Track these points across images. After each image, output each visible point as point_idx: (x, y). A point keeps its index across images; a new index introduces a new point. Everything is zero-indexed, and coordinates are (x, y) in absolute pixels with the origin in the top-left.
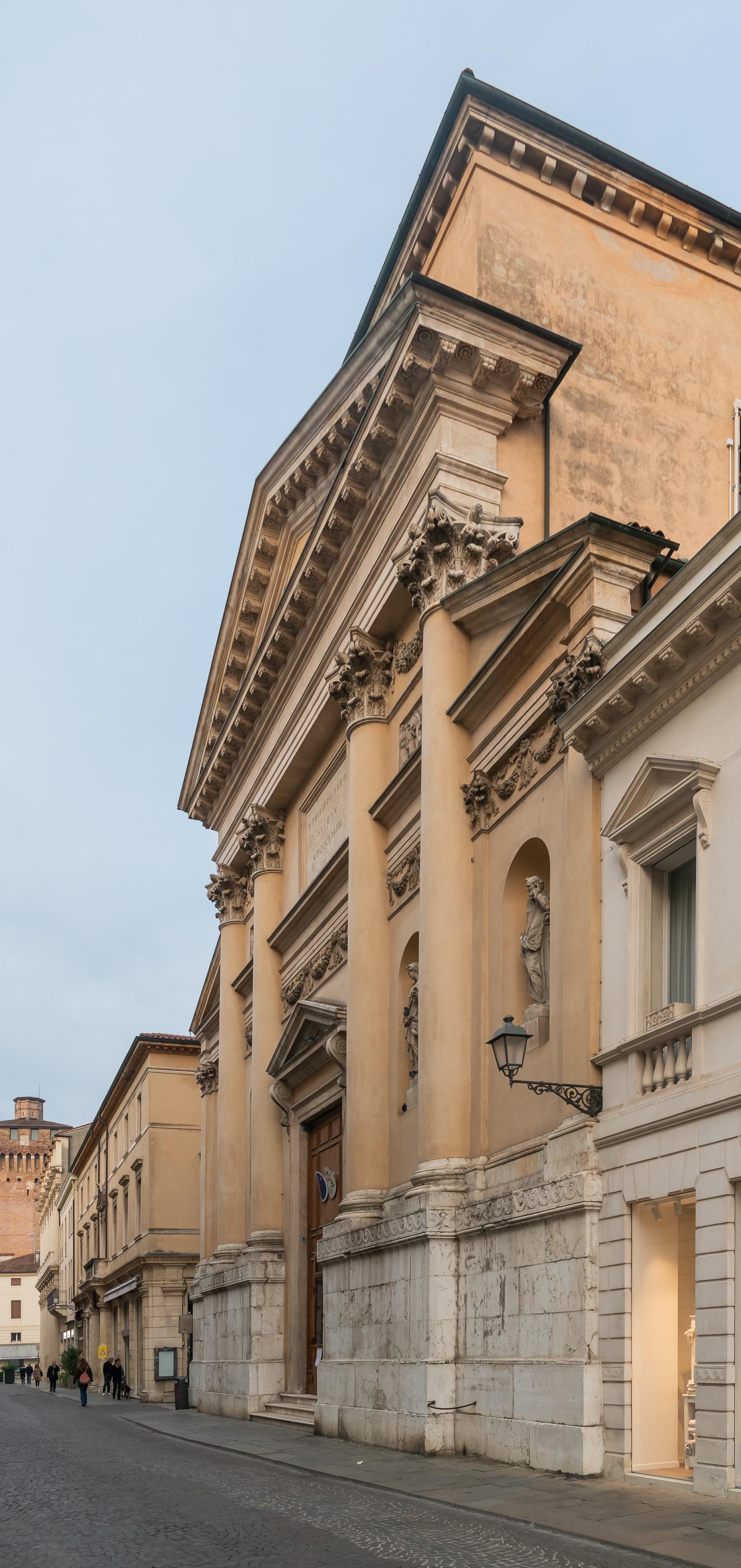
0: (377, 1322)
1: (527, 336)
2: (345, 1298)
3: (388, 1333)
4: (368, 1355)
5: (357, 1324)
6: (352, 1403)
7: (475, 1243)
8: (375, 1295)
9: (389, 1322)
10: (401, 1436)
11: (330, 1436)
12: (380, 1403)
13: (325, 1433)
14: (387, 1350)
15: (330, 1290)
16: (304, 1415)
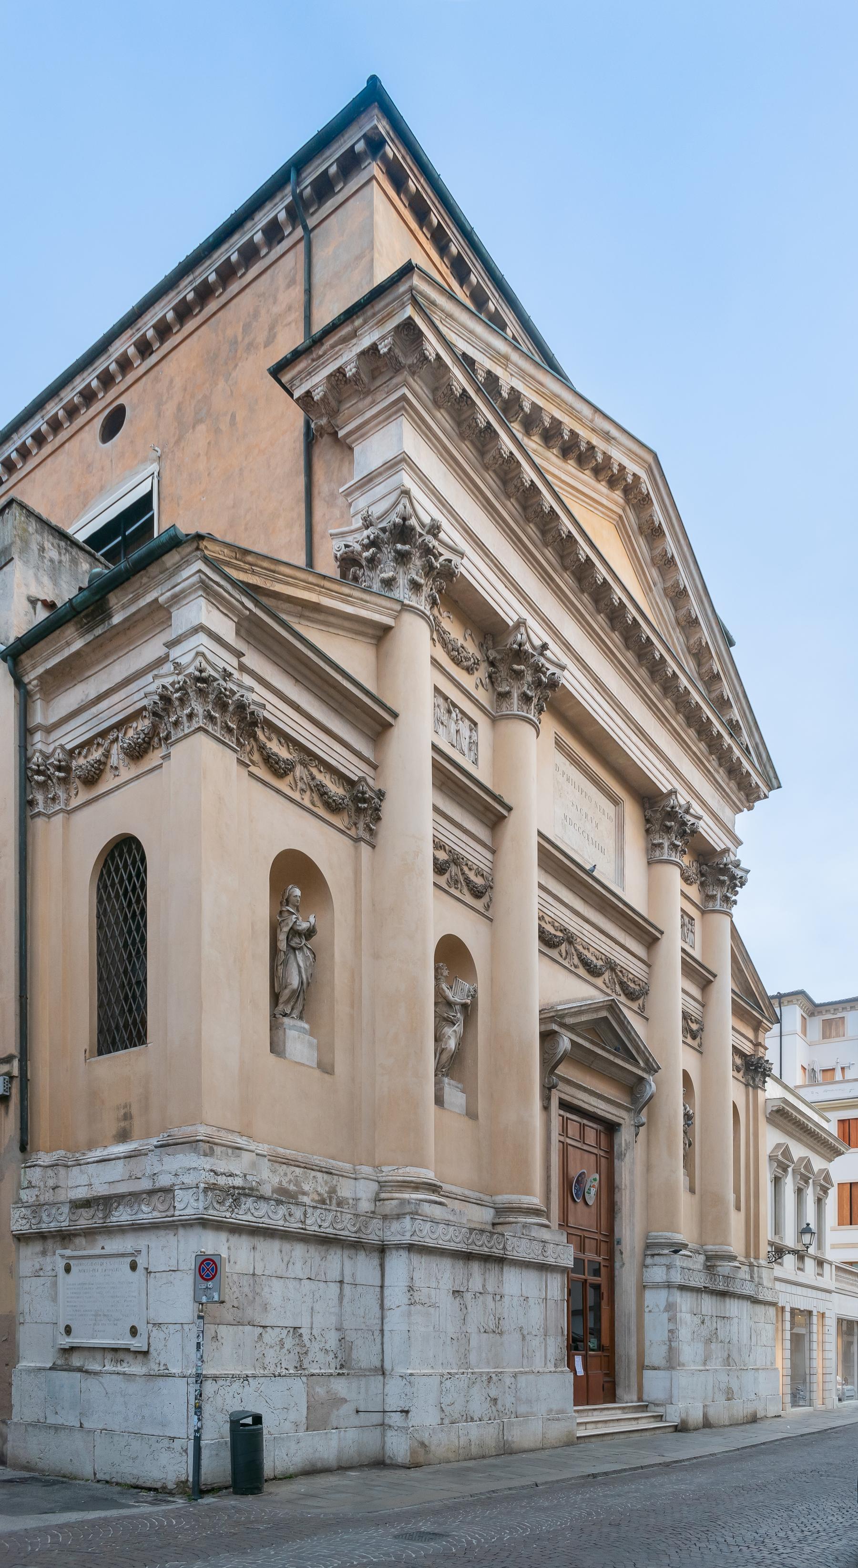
0: (721, 1342)
1: (289, 370)
2: (697, 1320)
3: (729, 1350)
4: (715, 1364)
5: (709, 1341)
6: (710, 1399)
7: (332, 1252)
8: (720, 1323)
9: (729, 1342)
10: (745, 1414)
11: (696, 1429)
12: (730, 1396)
13: (692, 1428)
14: (728, 1360)
15: (684, 1309)
16: (611, 1424)
